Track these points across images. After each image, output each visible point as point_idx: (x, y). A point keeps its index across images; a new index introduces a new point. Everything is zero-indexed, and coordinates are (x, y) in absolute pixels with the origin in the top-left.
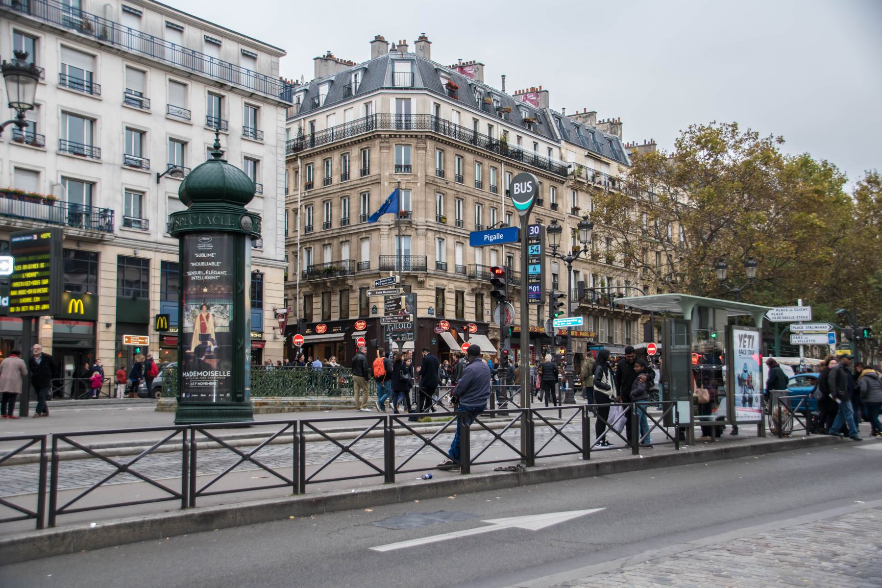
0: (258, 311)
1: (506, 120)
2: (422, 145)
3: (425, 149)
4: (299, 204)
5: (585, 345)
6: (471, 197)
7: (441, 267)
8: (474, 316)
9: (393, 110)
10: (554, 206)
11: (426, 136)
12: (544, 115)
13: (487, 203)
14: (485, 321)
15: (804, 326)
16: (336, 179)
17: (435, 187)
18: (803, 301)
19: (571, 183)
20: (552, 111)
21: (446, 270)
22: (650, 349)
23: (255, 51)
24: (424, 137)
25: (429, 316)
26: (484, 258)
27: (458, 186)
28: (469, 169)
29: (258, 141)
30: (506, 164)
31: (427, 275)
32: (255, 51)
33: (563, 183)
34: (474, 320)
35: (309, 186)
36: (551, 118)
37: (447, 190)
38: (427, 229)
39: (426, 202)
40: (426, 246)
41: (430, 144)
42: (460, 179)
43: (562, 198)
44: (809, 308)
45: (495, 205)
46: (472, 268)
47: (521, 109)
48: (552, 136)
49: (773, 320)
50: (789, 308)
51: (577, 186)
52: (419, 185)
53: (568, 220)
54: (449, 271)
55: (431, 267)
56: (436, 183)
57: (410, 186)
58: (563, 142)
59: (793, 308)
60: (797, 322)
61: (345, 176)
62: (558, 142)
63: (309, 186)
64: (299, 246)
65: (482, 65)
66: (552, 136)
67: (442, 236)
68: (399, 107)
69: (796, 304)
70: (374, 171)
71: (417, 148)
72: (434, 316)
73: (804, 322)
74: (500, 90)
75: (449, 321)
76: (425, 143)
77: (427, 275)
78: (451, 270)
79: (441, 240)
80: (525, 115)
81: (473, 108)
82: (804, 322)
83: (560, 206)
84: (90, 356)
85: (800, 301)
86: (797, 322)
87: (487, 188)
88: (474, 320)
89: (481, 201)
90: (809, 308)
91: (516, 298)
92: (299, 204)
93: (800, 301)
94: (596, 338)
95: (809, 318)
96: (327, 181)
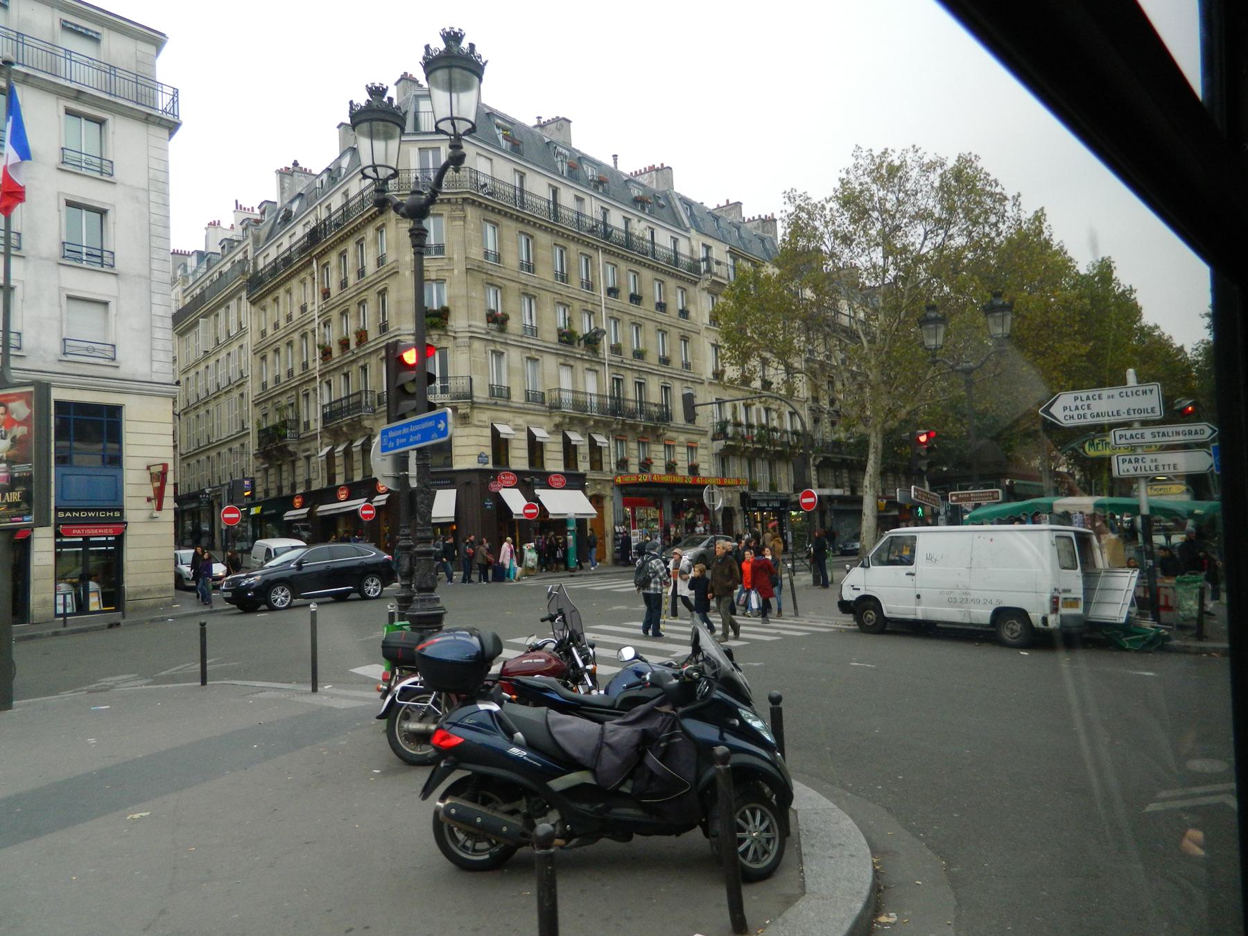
0: (110, 471)
1: (606, 193)
2: (458, 213)
3: (464, 218)
4: (317, 321)
5: (737, 496)
6: (549, 294)
7: (500, 395)
8: (562, 463)
9: (414, 163)
10: (684, 313)
11: (464, 199)
12: (667, 197)
13: (577, 305)
14: (581, 470)
15: (1148, 432)
16: (352, 279)
17: (484, 276)
18: (1137, 375)
19: (707, 284)
20: (678, 194)
21: (509, 398)
22: (805, 501)
23: (97, 28)
24: (460, 201)
25: (481, 466)
26: (574, 381)
27: (524, 276)
28: (543, 254)
29: (105, 177)
30: (605, 251)
31: (473, 405)
32: (97, 28)
33: (696, 283)
34: (562, 469)
35: (326, 294)
36: (678, 202)
37: (505, 282)
38: (471, 337)
39: (468, 297)
40: (472, 363)
41: (470, 211)
42: (529, 267)
43: (695, 303)
44: (1156, 387)
45: (590, 307)
46: (555, 394)
47: (631, 185)
48: (678, 223)
49: (1067, 423)
50: (1105, 392)
51: (716, 289)
52: (456, 272)
53: (704, 333)
54: (513, 399)
55: (481, 394)
56: (484, 272)
57: (442, 275)
58: (693, 232)
59: (1115, 391)
60: (1127, 425)
61: (361, 273)
62: (687, 230)
63: (326, 294)
64: (318, 380)
65: (569, 122)
66: (678, 223)
67: (499, 347)
68: (423, 159)
69: (1123, 382)
70: (390, 258)
71: (453, 218)
72: (490, 466)
73: (1145, 423)
74: (612, 165)
75: (516, 472)
76: (463, 210)
77: (473, 405)
78: (517, 397)
79: (499, 354)
80: (636, 192)
81: (548, 171)
82: (1145, 423)
83: (692, 314)
84: (1106, 464)
85: (1131, 374)
86: (1127, 425)
87: (575, 282)
88: (562, 469)
89: (567, 301)
90: (1156, 387)
91: (630, 438)
92: (317, 321)
93: (1131, 374)
94: (753, 486)
95: (1158, 414)
96: (344, 284)
